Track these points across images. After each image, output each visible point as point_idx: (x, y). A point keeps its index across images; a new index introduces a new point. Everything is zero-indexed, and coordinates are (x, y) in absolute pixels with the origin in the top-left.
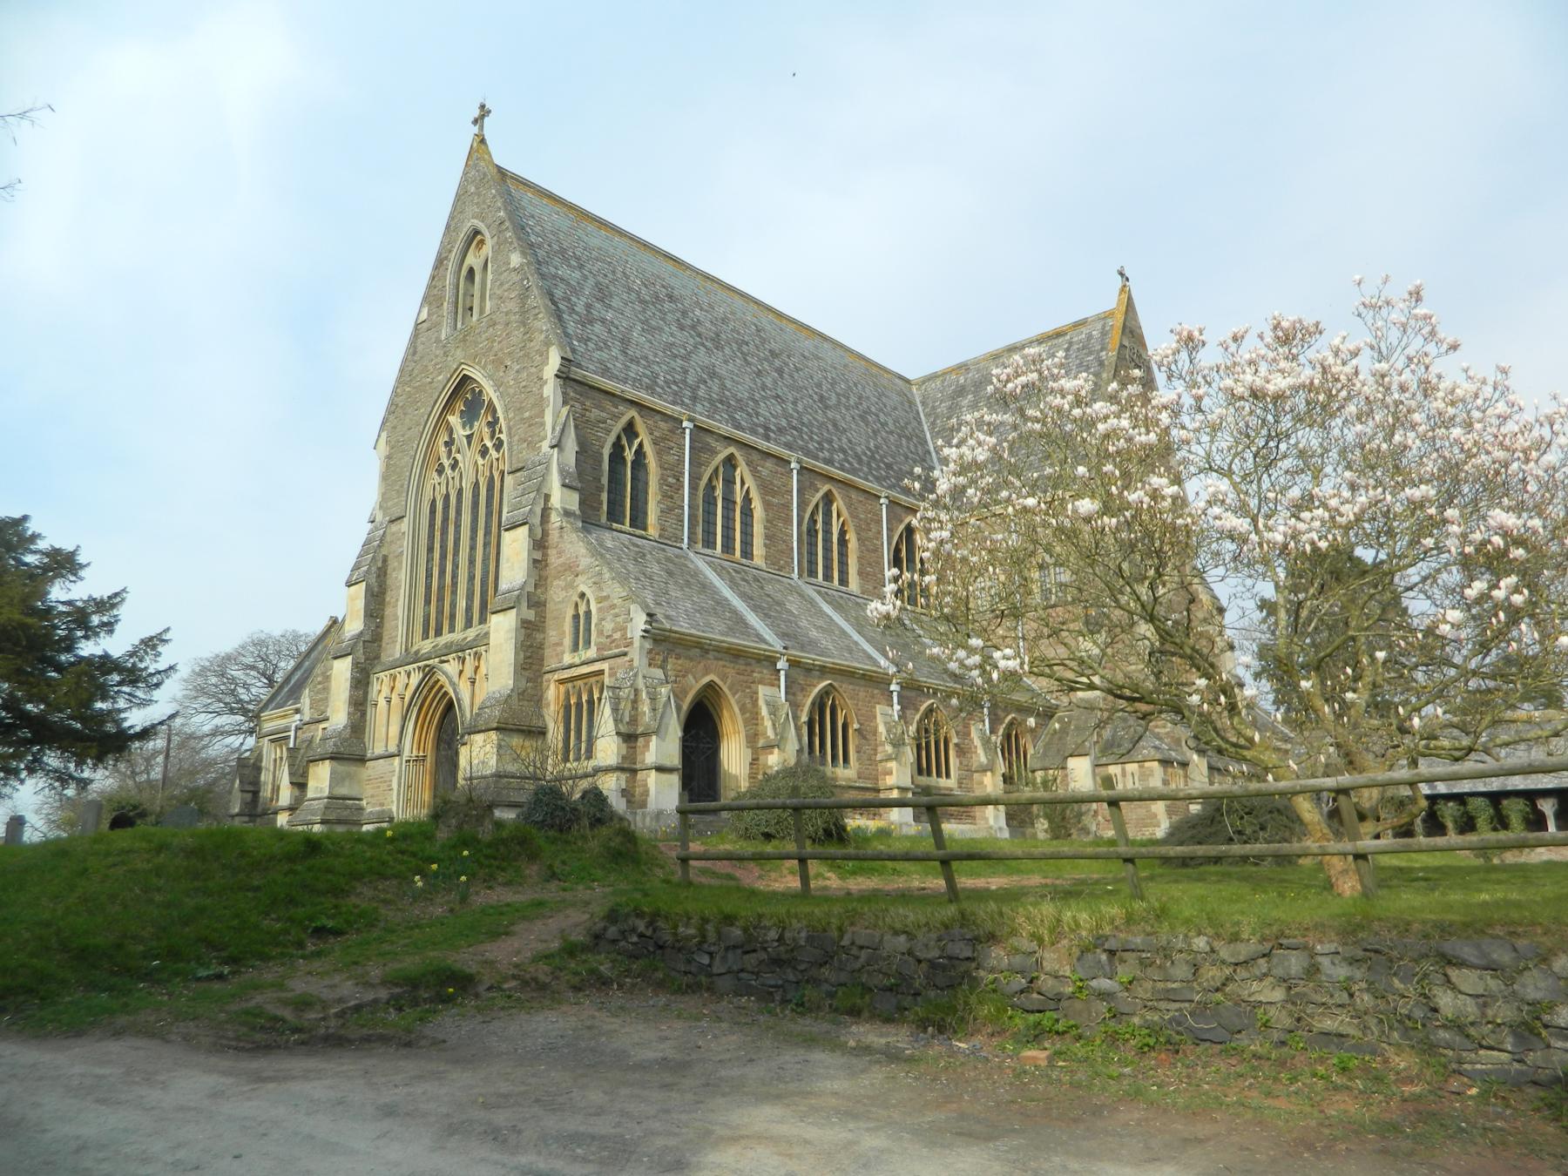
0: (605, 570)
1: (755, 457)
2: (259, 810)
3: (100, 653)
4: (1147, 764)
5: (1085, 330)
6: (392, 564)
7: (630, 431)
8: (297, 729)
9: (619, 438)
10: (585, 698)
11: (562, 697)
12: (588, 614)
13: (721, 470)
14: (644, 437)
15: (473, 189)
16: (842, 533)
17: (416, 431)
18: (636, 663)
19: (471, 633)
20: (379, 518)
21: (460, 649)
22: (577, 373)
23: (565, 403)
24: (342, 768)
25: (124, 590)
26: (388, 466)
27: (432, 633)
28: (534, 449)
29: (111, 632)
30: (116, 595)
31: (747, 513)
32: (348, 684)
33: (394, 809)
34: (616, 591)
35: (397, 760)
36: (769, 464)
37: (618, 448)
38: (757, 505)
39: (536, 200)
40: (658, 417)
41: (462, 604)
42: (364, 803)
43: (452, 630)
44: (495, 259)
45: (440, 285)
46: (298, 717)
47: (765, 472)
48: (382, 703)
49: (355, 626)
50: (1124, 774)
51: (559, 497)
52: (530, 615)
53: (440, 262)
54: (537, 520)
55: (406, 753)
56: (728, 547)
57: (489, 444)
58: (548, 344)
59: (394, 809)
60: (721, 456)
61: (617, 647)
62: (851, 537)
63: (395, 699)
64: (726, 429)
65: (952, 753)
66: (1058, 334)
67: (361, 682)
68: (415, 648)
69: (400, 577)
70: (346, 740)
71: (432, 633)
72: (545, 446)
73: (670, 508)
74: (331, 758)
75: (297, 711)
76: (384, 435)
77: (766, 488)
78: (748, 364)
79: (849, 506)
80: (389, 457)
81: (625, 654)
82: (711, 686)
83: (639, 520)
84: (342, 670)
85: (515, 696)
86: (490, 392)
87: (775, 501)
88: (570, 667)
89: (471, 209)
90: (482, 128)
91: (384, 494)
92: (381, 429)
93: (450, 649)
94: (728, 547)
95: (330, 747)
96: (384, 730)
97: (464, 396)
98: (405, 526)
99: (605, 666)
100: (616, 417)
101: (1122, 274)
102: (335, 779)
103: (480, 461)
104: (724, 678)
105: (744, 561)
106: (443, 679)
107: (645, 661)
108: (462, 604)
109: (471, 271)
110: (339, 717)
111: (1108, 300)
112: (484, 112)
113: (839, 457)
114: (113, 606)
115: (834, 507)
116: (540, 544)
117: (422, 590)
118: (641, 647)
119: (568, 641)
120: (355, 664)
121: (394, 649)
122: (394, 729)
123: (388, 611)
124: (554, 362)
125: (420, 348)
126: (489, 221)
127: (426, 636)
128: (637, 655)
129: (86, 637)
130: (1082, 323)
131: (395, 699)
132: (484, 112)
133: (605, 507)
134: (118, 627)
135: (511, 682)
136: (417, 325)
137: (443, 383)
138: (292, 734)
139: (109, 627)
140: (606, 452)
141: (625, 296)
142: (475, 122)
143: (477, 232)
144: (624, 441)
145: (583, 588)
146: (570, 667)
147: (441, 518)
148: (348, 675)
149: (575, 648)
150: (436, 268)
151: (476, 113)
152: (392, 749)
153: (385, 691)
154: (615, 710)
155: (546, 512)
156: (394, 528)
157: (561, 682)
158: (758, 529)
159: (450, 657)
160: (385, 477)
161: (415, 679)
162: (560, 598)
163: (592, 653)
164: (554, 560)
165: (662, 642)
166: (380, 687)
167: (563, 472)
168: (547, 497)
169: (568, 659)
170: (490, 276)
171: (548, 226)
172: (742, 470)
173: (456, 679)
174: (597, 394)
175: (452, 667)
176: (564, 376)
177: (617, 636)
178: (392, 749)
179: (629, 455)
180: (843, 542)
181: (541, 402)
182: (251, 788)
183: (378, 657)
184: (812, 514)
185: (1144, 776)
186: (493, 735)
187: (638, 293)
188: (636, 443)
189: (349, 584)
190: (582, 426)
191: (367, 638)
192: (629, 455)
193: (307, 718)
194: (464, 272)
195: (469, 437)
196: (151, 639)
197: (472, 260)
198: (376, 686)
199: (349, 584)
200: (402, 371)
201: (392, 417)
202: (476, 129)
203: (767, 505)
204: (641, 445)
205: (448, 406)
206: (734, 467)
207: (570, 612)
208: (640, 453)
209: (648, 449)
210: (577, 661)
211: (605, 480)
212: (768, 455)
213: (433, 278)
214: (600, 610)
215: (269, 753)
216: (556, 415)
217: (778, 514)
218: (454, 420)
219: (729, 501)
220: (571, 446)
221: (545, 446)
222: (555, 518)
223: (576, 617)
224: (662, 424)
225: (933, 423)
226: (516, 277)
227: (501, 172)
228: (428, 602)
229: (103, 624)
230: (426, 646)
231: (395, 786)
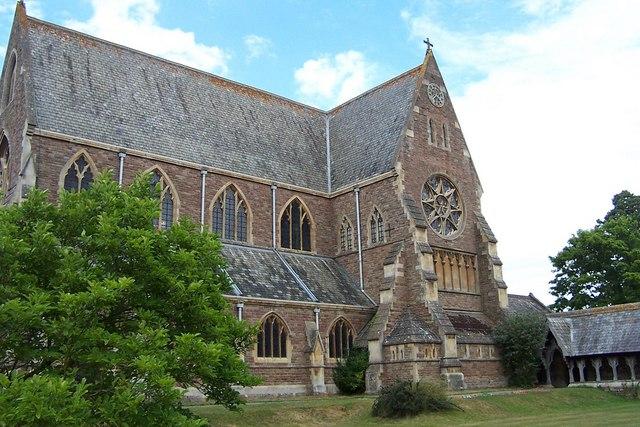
9: (73, 166)
22: (40, 131)
64: (150, 155)
77: (181, 187)
140: (63, 174)
144: (77, 168)
203: (182, 197)
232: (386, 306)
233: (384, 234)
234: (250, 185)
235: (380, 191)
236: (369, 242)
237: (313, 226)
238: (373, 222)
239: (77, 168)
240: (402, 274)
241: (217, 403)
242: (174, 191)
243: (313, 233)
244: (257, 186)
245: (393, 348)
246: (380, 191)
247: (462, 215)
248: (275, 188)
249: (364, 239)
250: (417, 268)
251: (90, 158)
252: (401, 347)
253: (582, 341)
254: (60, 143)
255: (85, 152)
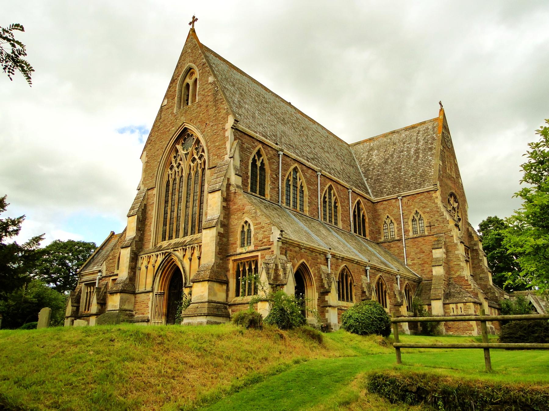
0: (258, 211)
1: (305, 168)
2: (79, 314)
3: (11, 243)
4: (467, 304)
5: (425, 126)
6: (149, 208)
7: (259, 154)
8: (100, 279)
9: (255, 156)
10: (247, 268)
11: (235, 267)
12: (249, 231)
13: (292, 173)
14: (264, 157)
15: (190, 51)
16: (335, 203)
17: (160, 152)
18: (275, 253)
19: (188, 239)
20: (142, 188)
21: (184, 246)
22: (241, 127)
23: (235, 140)
24: (125, 296)
25: (24, 216)
26: (146, 166)
27: (167, 238)
28: (220, 158)
29: (17, 234)
30: (21, 218)
31: (302, 192)
32: (128, 260)
33: (150, 316)
34: (263, 220)
35: (151, 294)
36: (310, 171)
37: (254, 161)
38: (305, 189)
39: (214, 57)
40: (269, 149)
41: (182, 226)
42: (134, 313)
43: (177, 237)
44: (200, 80)
45: (173, 90)
46: (99, 274)
47: (308, 175)
48: (143, 268)
49: (132, 234)
50: (457, 308)
51: (235, 180)
52: (222, 230)
53: (173, 81)
54: (224, 189)
55: (155, 291)
56: (295, 206)
57: (197, 157)
58: (227, 114)
59: (150, 316)
60: (292, 167)
61: (265, 245)
62: (339, 205)
63: (150, 266)
64: (294, 156)
65: (387, 297)
66: (413, 127)
67: (134, 258)
68: (159, 245)
69: (153, 214)
70: (127, 284)
71: (167, 238)
72: (227, 157)
73: (275, 188)
74: (120, 292)
75: (100, 271)
76: (145, 153)
77: (309, 183)
78: (296, 132)
79: (338, 191)
80: (147, 162)
81: (270, 248)
82: (303, 264)
83: (262, 193)
84: (126, 254)
85: (215, 267)
86: (198, 134)
87: (312, 188)
88: (240, 254)
89: (188, 59)
90: (193, 26)
91: (144, 178)
92: (144, 151)
93: (176, 246)
94: (295, 206)
95: (120, 287)
96: (144, 281)
97: (184, 135)
98: (155, 191)
99: (259, 254)
100: (254, 147)
101: (440, 104)
102: (122, 302)
103: (192, 164)
104: (308, 261)
105: (301, 212)
106: (175, 258)
107: (279, 252)
108: (182, 226)
109: (188, 85)
110: (123, 274)
111: (436, 114)
112: (195, 20)
113: (332, 172)
114: (19, 222)
115: (332, 192)
116: (227, 200)
117: (162, 219)
118: (278, 245)
119: (239, 242)
120: (132, 251)
121: (150, 246)
122: (150, 280)
123: (147, 228)
124: (231, 121)
125: (163, 116)
126: (197, 64)
127: (164, 239)
128: (276, 248)
129: (6, 235)
130: (424, 123)
131: (150, 266)
132: (195, 20)
133: (250, 185)
134: (20, 232)
135: (214, 260)
136: (162, 107)
137: (174, 131)
138: (97, 281)
139: (16, 232)
140: (250, 161)
141: (250, 99)
142: (190, 24)
143: (191, 69)
144: (256, 158)
145: (246, 219)
146: (240, 254)
147: (169, 190)
148: (129, 256)
149: (243, 245)
150: (171, 83)
151: (191, 20)
152: (149, 288)
153: (145, 263)
154: (268, 273)
155: (229, 185)
156: (150, 192)
157: (235, 261)
158: (306, 199)
159: (179, 249)
160: (145, 171)
161: (160, 259)
162: (237, 224)
163: (252, 248)
164: (233, 207)
165: (287, 245)
166: (143, 263)
167: (235, 168)
168: (228, 179)
169: (239, 250)
170: (198, 86)
171: (220, 68)
172: (300, 174)
173: (181, 258)
174: (246, 136)
175: (180, 254)
176: (235, 128)
177: (265, 240)
178: (149, 288)
179: (259, 164)
180: (336, 207)
181: (224, 138)
182: (76, 305)
183: (141, 248)
184: (325, 194)
185: (466, 309)
186: (206, 284)
187: (255, 98)
188: (261, 158)
189: (129, 216)
190: (242, 149)
191: (137, 239)
192: (259, 164)
193: (104, 275)
194: (184, 85)
195: (186, 154)
196: (36, 238)
197: (189, 81)
198: (140, 261)
199: (129, 216)
200: (154, 126)
201: (149, 146)
202: (191, 26)
203: (309, 189)
204: (263, 160)
205: (177, 141)
206: (297, 172)
207: (240, 229)
208: (262, 164)
209: (266, 162)
210: (244, 251)
211: (250, 174)
212: (309, 168)
213: (170, 87)
214: (255, 229)
215: (84, 289)
216: (232, 145)
217: (314, 193)
218: (179, 147)
219: (295, 187)
220: (237, 156)
221: (227, 157)
222: (232, 189)
223: (243, 232)
224: (271, 152)
225: (361, 162)
226: (210, 87)
227: (202, 46)
228: (165, 224)
229: (14, 231)
230: (165, 244)
231: (150, 305)
232: (438, 278)
233: (426, 229)
234: (339, 186)
235: (421, 200)
236: (411, 234)
237: (367, 220)
238: (414, 220)
239: (256, 158)
240: (444, 256)
241: (384, 344)
242: (305, 184)
243: (367, 225)
244: (342, 188)
245: (451, 306)
246: (421, 200)
247: (461, 221)
248: (350, 191)
249: (406, 231)
250: (456, 252)
251: (264, 152)
252: (460, 305)
253: (29, 381)
254: (249, 138)
255: (262, 148)
